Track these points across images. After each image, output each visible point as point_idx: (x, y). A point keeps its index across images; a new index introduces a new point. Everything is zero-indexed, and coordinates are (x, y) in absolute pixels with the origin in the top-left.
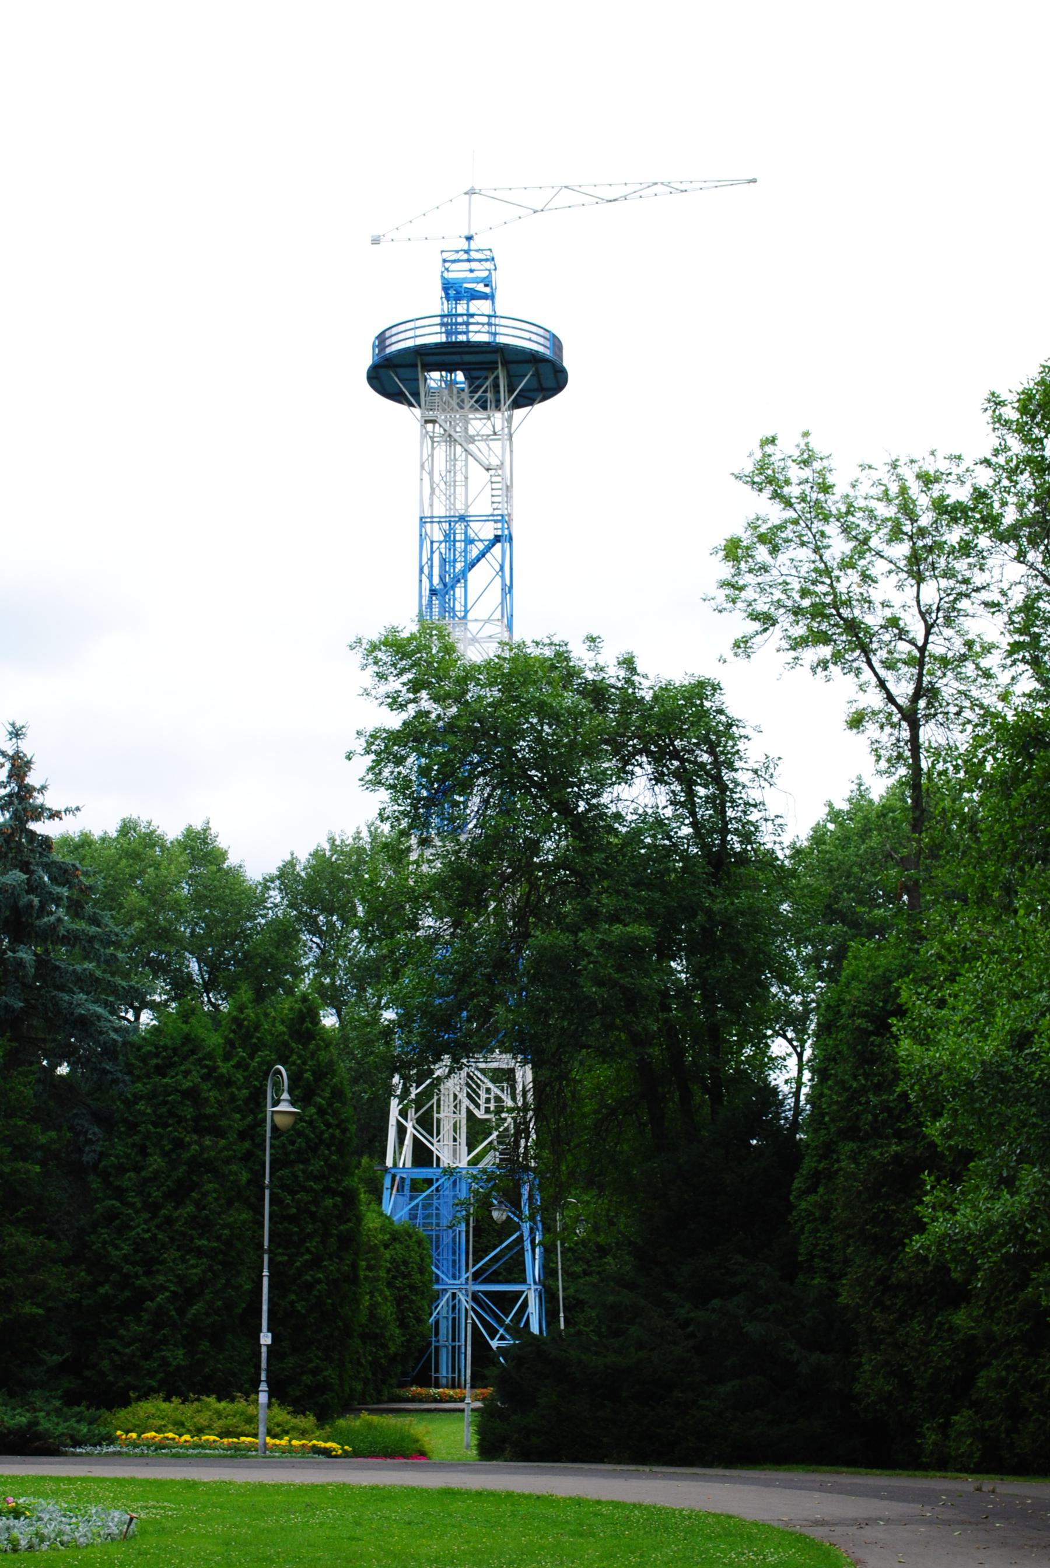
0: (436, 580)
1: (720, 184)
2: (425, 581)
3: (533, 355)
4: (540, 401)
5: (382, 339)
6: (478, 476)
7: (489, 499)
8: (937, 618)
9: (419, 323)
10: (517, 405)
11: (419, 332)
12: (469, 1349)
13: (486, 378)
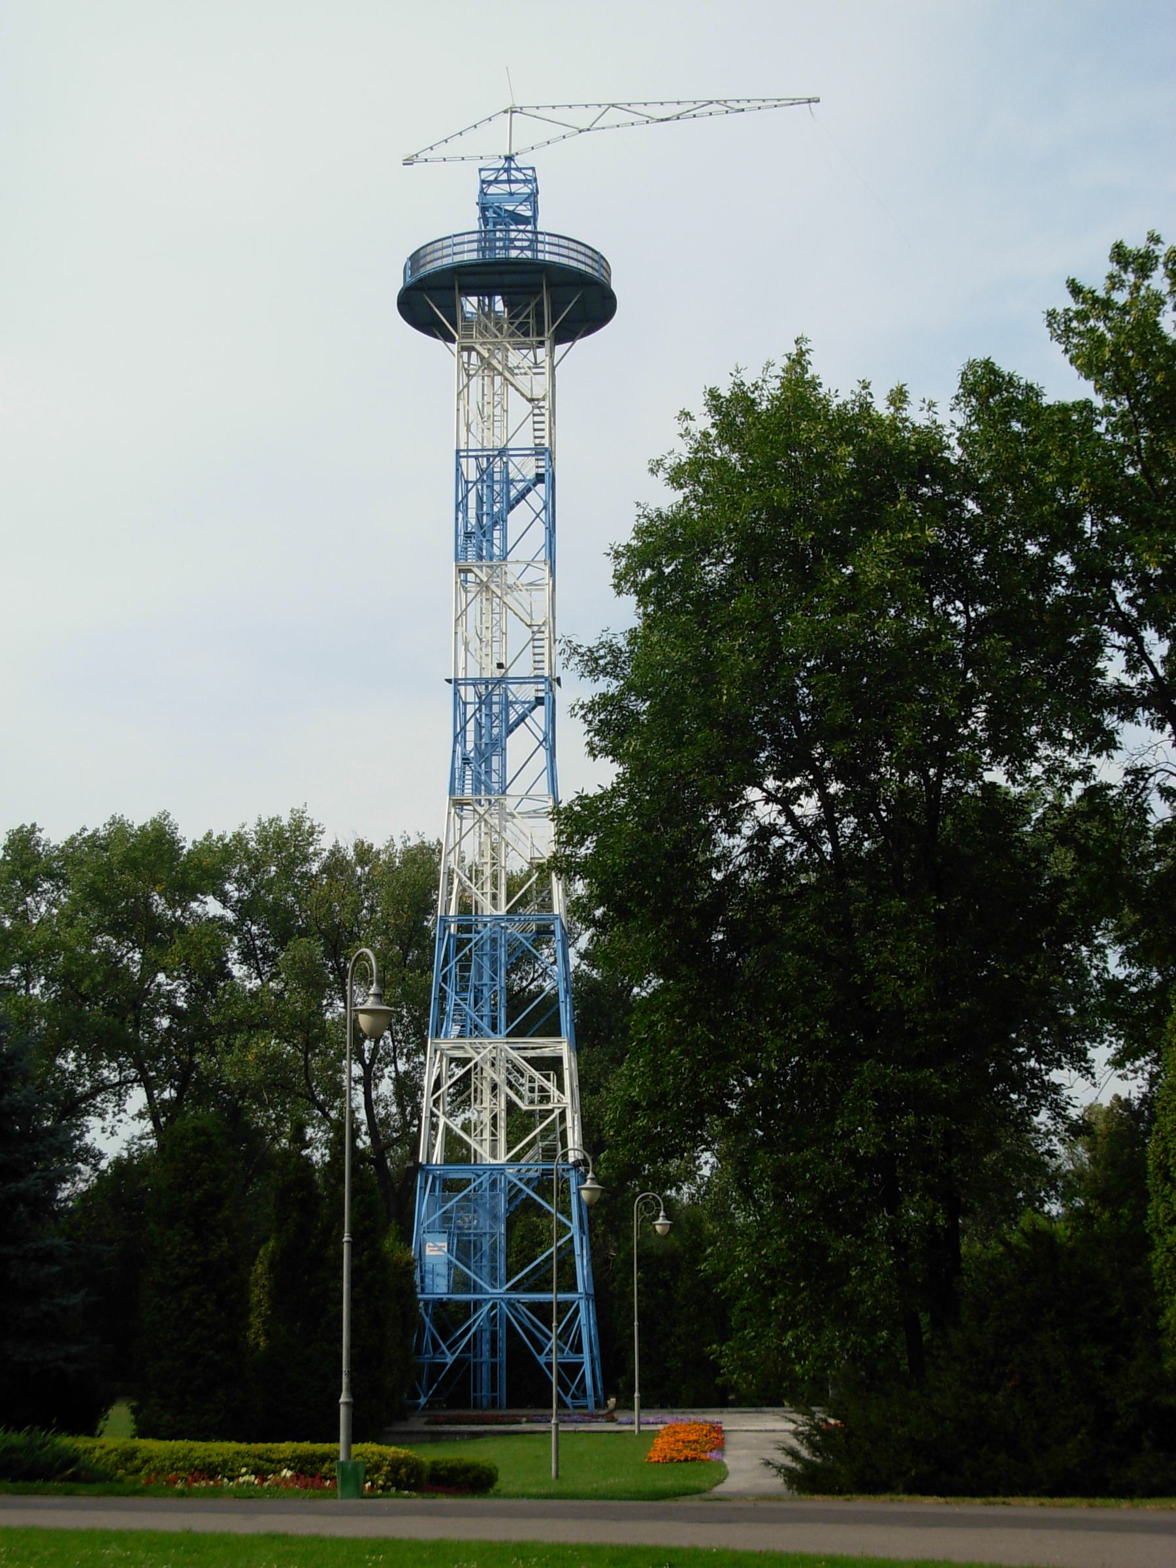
0: (470, 746)
1: (779, 103)
2: (459, 748)
3: (581, 275)
4: (582, 337)
5: (415, 259)
6: (519, 408)
7: (531, 658)
8: (1066, 858)
9: (457, 240)
10: (559, 339)
11: (457, 249)
12: (505, 1387)
13: (528, 305)
